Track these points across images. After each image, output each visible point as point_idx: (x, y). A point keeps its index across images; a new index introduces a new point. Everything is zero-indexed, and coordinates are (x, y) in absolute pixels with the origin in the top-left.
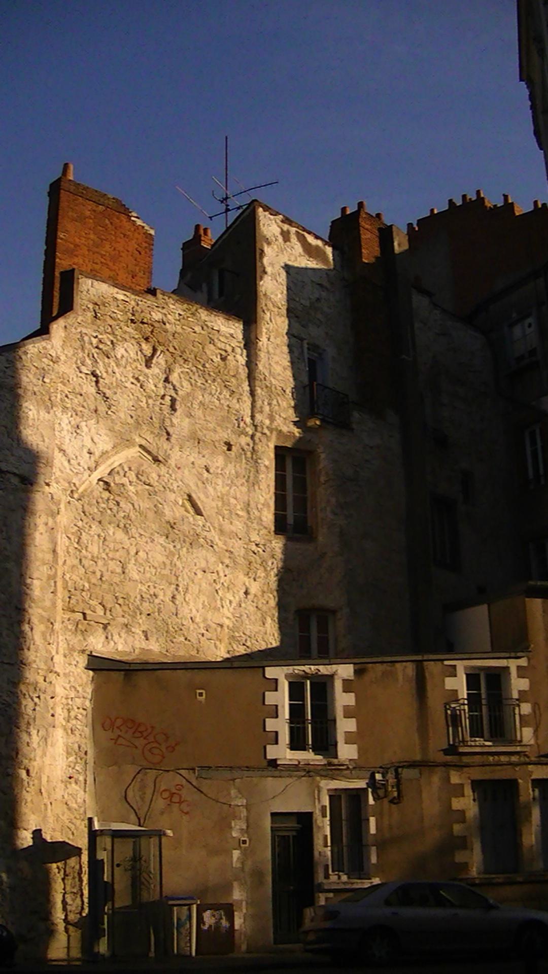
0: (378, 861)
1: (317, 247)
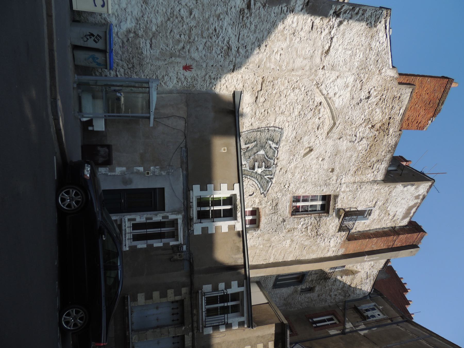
0: (125, 167)
1: (410, 213)
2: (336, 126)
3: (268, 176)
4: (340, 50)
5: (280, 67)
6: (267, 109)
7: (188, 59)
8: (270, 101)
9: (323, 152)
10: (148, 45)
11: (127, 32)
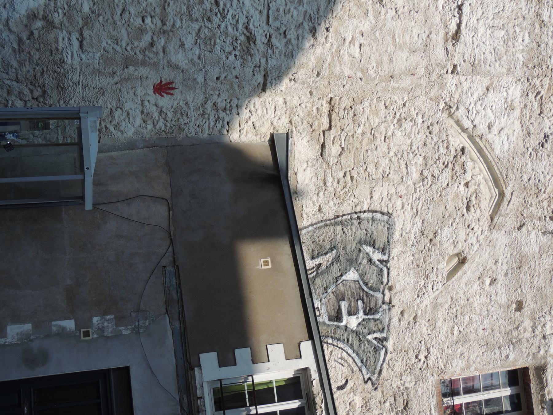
2: (505, 199)
3: (375, 335)
4: (481, 30)
5: (363, 71)
6: (348, 169)
7: (163, 68)
8: (352, 151)
9: (491, 262)
10: (76, 44)
11: (28, 19)
